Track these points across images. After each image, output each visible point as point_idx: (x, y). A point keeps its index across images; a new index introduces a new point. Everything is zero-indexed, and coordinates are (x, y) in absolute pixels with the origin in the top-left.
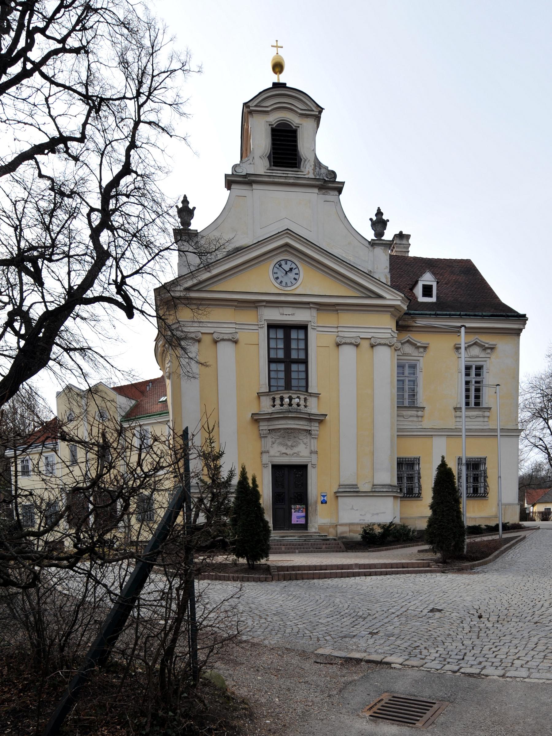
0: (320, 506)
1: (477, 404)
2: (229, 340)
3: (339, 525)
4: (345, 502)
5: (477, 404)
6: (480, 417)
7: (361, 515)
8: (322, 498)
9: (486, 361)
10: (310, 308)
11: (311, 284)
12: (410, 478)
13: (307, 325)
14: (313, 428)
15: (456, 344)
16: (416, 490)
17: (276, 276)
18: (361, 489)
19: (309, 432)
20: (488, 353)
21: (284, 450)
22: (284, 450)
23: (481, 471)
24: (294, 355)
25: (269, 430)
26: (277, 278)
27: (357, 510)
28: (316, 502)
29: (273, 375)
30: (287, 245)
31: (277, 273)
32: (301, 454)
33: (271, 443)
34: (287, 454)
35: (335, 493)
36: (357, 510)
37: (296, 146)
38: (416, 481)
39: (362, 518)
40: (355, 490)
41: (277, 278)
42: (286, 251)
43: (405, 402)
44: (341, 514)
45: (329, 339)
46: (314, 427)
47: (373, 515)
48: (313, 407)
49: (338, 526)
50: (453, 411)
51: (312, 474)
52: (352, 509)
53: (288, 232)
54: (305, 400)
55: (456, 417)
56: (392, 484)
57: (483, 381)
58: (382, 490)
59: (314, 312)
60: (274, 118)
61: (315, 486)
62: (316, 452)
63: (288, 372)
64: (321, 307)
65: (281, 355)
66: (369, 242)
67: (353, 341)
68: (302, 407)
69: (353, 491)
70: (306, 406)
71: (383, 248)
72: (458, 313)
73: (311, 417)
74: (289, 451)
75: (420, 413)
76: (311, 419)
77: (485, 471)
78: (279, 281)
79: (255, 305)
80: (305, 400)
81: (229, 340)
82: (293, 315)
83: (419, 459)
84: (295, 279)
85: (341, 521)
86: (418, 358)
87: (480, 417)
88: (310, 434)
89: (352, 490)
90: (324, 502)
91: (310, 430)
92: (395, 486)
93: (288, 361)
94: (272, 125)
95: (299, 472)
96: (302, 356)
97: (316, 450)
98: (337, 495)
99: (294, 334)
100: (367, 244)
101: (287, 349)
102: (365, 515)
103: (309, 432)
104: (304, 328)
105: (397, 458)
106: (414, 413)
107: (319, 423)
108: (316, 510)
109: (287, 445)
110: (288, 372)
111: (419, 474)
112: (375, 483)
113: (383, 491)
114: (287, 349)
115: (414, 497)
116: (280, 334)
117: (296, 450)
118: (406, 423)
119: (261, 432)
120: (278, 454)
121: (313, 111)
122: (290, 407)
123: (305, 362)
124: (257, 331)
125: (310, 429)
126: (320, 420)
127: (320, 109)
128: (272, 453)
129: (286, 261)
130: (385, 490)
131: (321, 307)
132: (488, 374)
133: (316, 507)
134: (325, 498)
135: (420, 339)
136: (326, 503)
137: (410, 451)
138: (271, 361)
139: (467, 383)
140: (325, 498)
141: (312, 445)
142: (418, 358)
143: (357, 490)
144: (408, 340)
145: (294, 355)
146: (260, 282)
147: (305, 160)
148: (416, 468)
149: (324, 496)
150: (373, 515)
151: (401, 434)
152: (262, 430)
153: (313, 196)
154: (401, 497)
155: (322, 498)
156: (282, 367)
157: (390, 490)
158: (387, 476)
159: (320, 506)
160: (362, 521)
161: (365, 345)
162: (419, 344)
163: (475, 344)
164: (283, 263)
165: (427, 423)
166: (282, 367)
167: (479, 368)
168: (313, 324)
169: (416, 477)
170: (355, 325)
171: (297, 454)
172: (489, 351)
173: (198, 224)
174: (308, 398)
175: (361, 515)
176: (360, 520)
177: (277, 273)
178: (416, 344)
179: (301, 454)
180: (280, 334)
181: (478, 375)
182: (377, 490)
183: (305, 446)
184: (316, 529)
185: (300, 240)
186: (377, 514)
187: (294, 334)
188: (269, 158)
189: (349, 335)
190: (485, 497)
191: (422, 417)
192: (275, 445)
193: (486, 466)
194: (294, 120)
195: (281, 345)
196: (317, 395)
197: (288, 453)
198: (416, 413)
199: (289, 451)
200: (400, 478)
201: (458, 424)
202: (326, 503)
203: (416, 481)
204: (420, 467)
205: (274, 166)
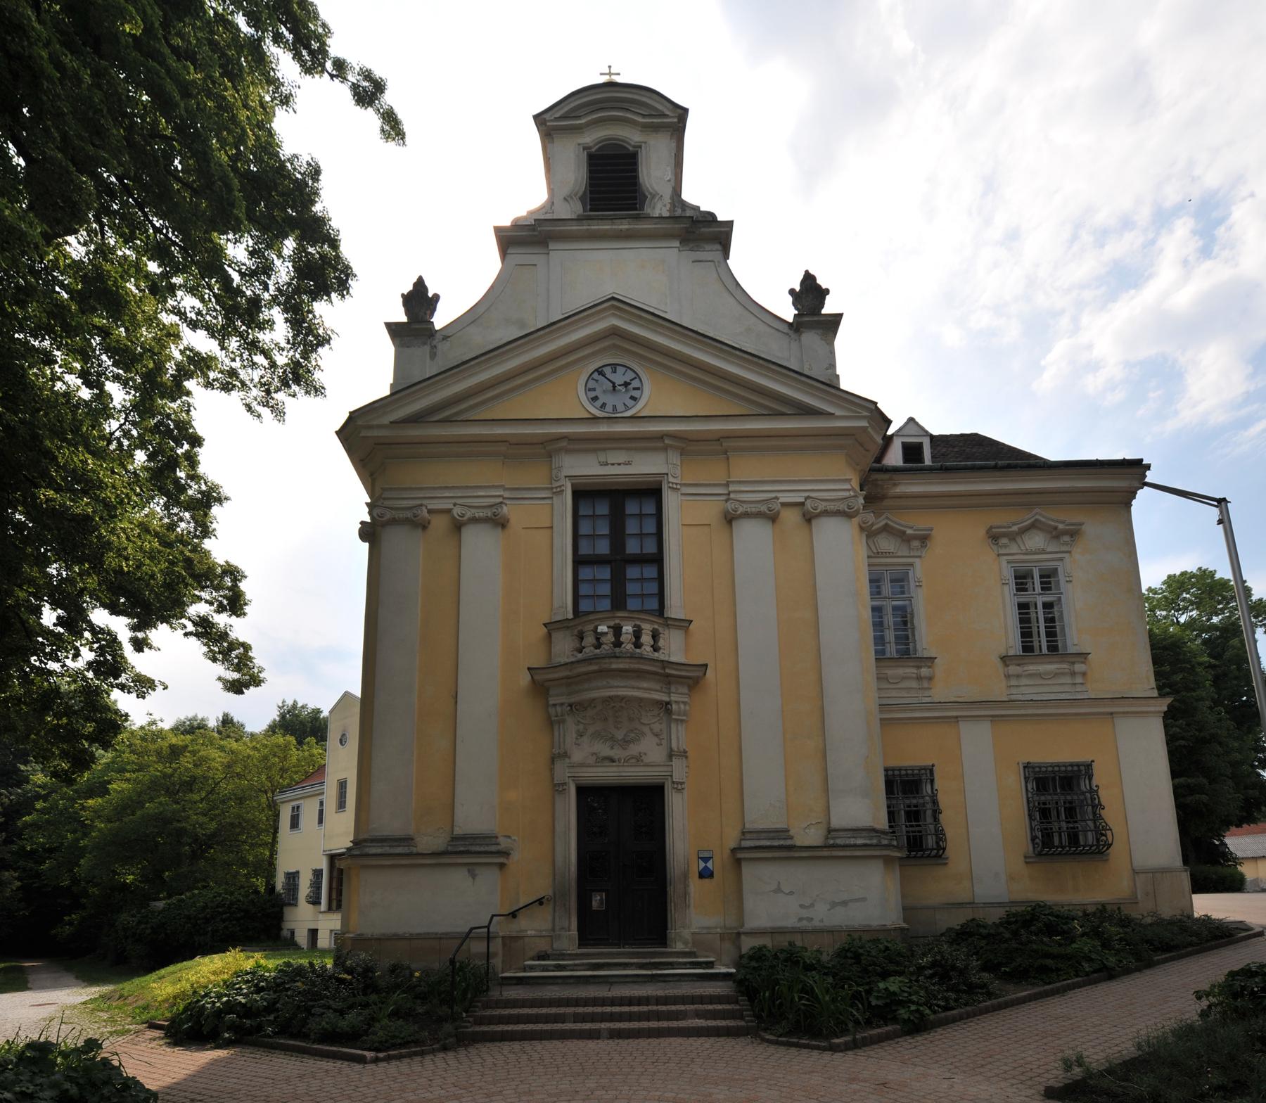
0: (695, 885)
1: (1053, 648)
2: (485, 520)
3: (746, 934)
4: (759, 877)
5: (1053, 648)
6: (1063, 674)
7: (801, 906)
8: (702, 865)
9: (1061, 559)
10: (665, 449)
11: (661, 399)
12: (914, 815)
13: (660, 483)
14: (674, 698)
15: (991, 527)
16: (930, 841)
17: (592, 394)
18: (798, 841)
19: (666, 707)
20: (1066, 544)
21: (605, 750)
22: (605, 750)
23: (1083, 793)
24: (632, 547)
25: (570, 705)
26: (595, 399)
27: (791, 893)
28: (686, 876)
29: (584, 589)
30: (614, 332)
31: (594, 390)
32: (646, 759)
33: (574, 736)
34: (613, 761)
35: (734, 851)
36: (791, 893)
37: (636, 177)
38: (929, 820)
39: (804, 913)
40: (782, 842)
41: (595, 399)
42: (615, 346)
43: (888, 649)
44: (749, 903)
45: (710, 510)
46: (677, 696)
47: (834, 905)
48: (674, 648)
49: (743, 937)
50: (1000, 664)
51: (678, 810)
52: (778, 890)
53: (615, 304)
54: (655, 636)
55: (1008, 677)
56: (878, 826)
57: (1060, 599)
58: (852, 841)
59: (675, 458)
60: (591, 138)
61: (687, 832)
62: (684, 754)
63: (618, 583)
64: (687, 445)
65: (603, 548)
66: (790, 325)
67: (763, 508)
68: (647, 649)
69: (776, 847)
70: (656, 649)
71: (820, 332)
72: (993, 463)
73: (668, 671)
74: (616, 753)
75: (924, 671)
76: (668, 674)
77: (1093, 792)
78: (598, 403)
79: (546, 449)
80: (655, 636)
81: (485, 520)
82: (629, 463)
83: (931, 771)
84: (633, 398)
85: (752, 923)
86: (910, 560)
87: (1063, 674)
88: (669, 712)
89: (776, 843)
90: (705, 874)
91: (668, 703)
92: (883, 832)
93: (618, 561)
94: (590, 148)
95: (646, 801)
96: (650, 548)
97: (683, 746)
98: (738, 857)
99: (631, 508)
100: (785, 329)
101: (618, 536)
102: (812, 905)
103: (666, 707)
104: (652, 492)
105: (886, 770)
106: (911, 671)
107: (691, 688)
108: (686, 894)
109: (612, 739)
110: (618, 583)
111: (935, 802)
112: (835, 823)
113: (855, 846)
114: (618, 536)
115: (929, 856)
116: (603, 508)
117: (634, 749)
118: (894, 694)
119: (552, 711)
120: (591, 760)
121: (665, 116)
122: (617, 650)
123: (657, 559)
124: (549, 501)
125: (666, 699)
126: (691, 677)
127: (680, 111)
128: (577, 756)
129: (614, 367)
130: (859, 841)
131: (687, 445)
132: (1069, 585)
133: (686, 886)
134: (710, 865)
135: (914, 522)
136: (711, 875)
137: (912, 756)
138: (579, 561)
139: (1023, 606)
140: (710, 865)
141: (674, 737)
142: (910, 560)
143: (789, 842)
144: (886, 524)
145: (632, 547)
146: (566, 400)
147: (653, 196)
148: (1084, 786)
149: (706, 860)
150: (834, 905)
151: (890, 719)
152: (554, 705)
153: (670, 254)
154: (901, 858)
155: (702, 865)
156: (605, 573)
157: (875, 841)
158: (864, 808)
159: (695, 885)
160: (805, 923)
161: (791, 518)
162: (909, 532)
163: (1034, 526)
164: (608, 371)
165: (940, 692)
166: (605, 573)
167: (1048, 578)
168: (671, 479)
169: (929, 813)
170: (757, 477)
171: (638, 759)
172: (1066, 538)
173: (441, 318)
174: (661, 630)
175: (801, 906)
176: (801, 919)
177: (594, 390)
178: (904, 532)
179: (646, 759)
180: (603, 508)
181: (1046, 587)
182: (839, 842)
183: (656, 740)
184: (686, 943)
185: (640, 317)
186: (845, 903)
187: (631, 508)
188: (582, 199)
189: (751, 496)
190: (938, 856)
191: (930, 679)
192: (585, 739)
193: (1094, 783)
194: (632, 136)
195: (603, 528)
196: (684, 625)
197: (616, 757)
198: (915, 671)
199: (616, 753)
200: (891, 815)
201: (1014, 691)
202: (711, 875)
203: (929, 820)
204: (936, 787)
205: (591, 210)
